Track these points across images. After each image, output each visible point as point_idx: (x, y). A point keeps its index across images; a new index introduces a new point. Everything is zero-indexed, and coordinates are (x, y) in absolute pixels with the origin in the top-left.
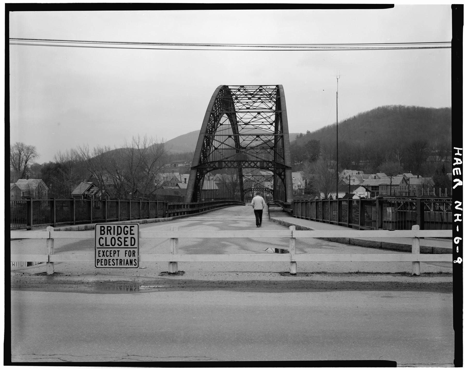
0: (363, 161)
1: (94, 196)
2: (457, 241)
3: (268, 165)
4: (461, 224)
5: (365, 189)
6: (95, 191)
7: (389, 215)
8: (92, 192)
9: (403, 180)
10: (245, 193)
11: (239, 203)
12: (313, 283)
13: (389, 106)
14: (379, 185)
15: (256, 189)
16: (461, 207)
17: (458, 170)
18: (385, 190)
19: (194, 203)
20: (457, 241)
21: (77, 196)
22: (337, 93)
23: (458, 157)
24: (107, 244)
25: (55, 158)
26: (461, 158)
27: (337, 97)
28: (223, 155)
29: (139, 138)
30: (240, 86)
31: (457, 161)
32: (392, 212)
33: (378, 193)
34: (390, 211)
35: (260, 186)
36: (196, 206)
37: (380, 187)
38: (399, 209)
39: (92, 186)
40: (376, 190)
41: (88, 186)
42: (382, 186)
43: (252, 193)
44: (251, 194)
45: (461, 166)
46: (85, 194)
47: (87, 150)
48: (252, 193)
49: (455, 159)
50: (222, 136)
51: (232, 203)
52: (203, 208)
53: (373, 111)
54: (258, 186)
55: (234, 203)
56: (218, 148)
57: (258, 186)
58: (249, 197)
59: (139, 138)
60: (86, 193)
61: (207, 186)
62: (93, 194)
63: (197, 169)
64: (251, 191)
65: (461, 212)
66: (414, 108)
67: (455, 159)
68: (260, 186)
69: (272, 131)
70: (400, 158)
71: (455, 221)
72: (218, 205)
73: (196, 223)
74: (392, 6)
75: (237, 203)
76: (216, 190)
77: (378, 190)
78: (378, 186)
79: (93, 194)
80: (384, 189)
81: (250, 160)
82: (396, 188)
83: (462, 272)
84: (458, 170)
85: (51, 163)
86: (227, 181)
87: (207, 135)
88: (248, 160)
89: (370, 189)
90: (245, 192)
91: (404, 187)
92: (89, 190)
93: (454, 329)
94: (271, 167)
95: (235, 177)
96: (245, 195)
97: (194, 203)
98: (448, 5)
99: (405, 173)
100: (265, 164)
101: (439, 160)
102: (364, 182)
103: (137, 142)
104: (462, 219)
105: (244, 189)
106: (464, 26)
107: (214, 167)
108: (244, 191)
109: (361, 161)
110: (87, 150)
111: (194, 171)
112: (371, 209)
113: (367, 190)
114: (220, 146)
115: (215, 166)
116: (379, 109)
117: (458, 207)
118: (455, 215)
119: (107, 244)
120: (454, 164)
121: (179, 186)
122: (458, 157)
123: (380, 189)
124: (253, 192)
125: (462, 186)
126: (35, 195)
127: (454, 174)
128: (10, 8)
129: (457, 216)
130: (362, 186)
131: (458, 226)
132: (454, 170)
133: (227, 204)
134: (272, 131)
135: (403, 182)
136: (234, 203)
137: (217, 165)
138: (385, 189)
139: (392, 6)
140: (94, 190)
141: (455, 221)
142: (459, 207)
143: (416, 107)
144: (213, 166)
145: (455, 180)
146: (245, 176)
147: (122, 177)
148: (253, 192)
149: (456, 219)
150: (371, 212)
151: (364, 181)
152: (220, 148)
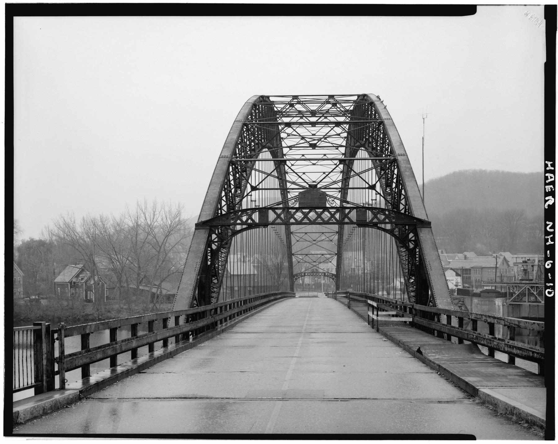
0: (441, 238)
1: (84, 284)
3: (375, 216)
5: (454, 273)
6: (86, 278)
7: (499, 309)
8: (82, 279)
9: (503, 261)
10: (296, 279)
11: (288, 295)
13: (467, 171)
14: (471, 267)
15: (312, 274)
18: (479, 273)
19: (202, 308)
20: (548, 265)
21: (62, 285)
22: (423, 138)
24: (18, 21)
25: (42, 234)
27: (423, 145)
29: (146, 203)
30: (293, 96)
31: (549, 177)
32: (503, 305)
33: (470, 278)
34: (500, 304)
35: (316, 270)
36: (208, 313)
37: (472, 269)
38: (512, 301)
39: (82, 271)
40: (467, 274)
41: (75, 271)
42: (475, 269)
47: (73, 220)
50: (263, 191)
51: (279, 296)
52: (225, 316)
53: (447, 177)
55: (283, 295)
56: (258, 187)
57: (314, 270)
59: (146, 203)
60: (74, 280)
62: (83, 281)
63: (211, 226)
65: (554, 233)
66: (497, 172)
70: (488, 235)
72: (257, 303)
74: (470, 10)
75: (286, 295)
76: (254, 275)
77: (470, 274)
78: (470, 270)
79: (83, 281)
80: (478, 273)
81: (333, 205)
82: (489, 271)
85: (32, 240)
86: (269, 263)
87: (234, 160)
88: (328, 206)
89: (459, 272)
90: (296, 277)
91: (505, 271)
92: (77, 276)
94: (383, 222)
96: (296, 282)
97: (202, 308)
99: (501, 251)
100: (369, 215)
101: (539, 236)
102: (450, 264)
103: (143, 208)
105: (294, 273)
107: (250, 221)
108: (294, 277)
109: (438, 238)
110: (73, 220)
111: (204, 231)
112: (472, 300)
113: (457, 275)
114: (261, 185)
115: (252, 220)
116: (455, 174)
119: (18, 21)
120: (547, 182)
123: (472, 272)
130: (451, 269)
132: (547, 187)
133: (272, 298)
135: (503, 264)
136: (283, 295)
137: (256, 217)
138: (479, 272)
139: (470, 10)
140: (84, 277)
142: (550, 228)
143: (501, 172)
144: (247, 220)
145: (547, 198)
147: (124, 258)
150: (471, 305)
151: (449, 262)
152: (261, 187)
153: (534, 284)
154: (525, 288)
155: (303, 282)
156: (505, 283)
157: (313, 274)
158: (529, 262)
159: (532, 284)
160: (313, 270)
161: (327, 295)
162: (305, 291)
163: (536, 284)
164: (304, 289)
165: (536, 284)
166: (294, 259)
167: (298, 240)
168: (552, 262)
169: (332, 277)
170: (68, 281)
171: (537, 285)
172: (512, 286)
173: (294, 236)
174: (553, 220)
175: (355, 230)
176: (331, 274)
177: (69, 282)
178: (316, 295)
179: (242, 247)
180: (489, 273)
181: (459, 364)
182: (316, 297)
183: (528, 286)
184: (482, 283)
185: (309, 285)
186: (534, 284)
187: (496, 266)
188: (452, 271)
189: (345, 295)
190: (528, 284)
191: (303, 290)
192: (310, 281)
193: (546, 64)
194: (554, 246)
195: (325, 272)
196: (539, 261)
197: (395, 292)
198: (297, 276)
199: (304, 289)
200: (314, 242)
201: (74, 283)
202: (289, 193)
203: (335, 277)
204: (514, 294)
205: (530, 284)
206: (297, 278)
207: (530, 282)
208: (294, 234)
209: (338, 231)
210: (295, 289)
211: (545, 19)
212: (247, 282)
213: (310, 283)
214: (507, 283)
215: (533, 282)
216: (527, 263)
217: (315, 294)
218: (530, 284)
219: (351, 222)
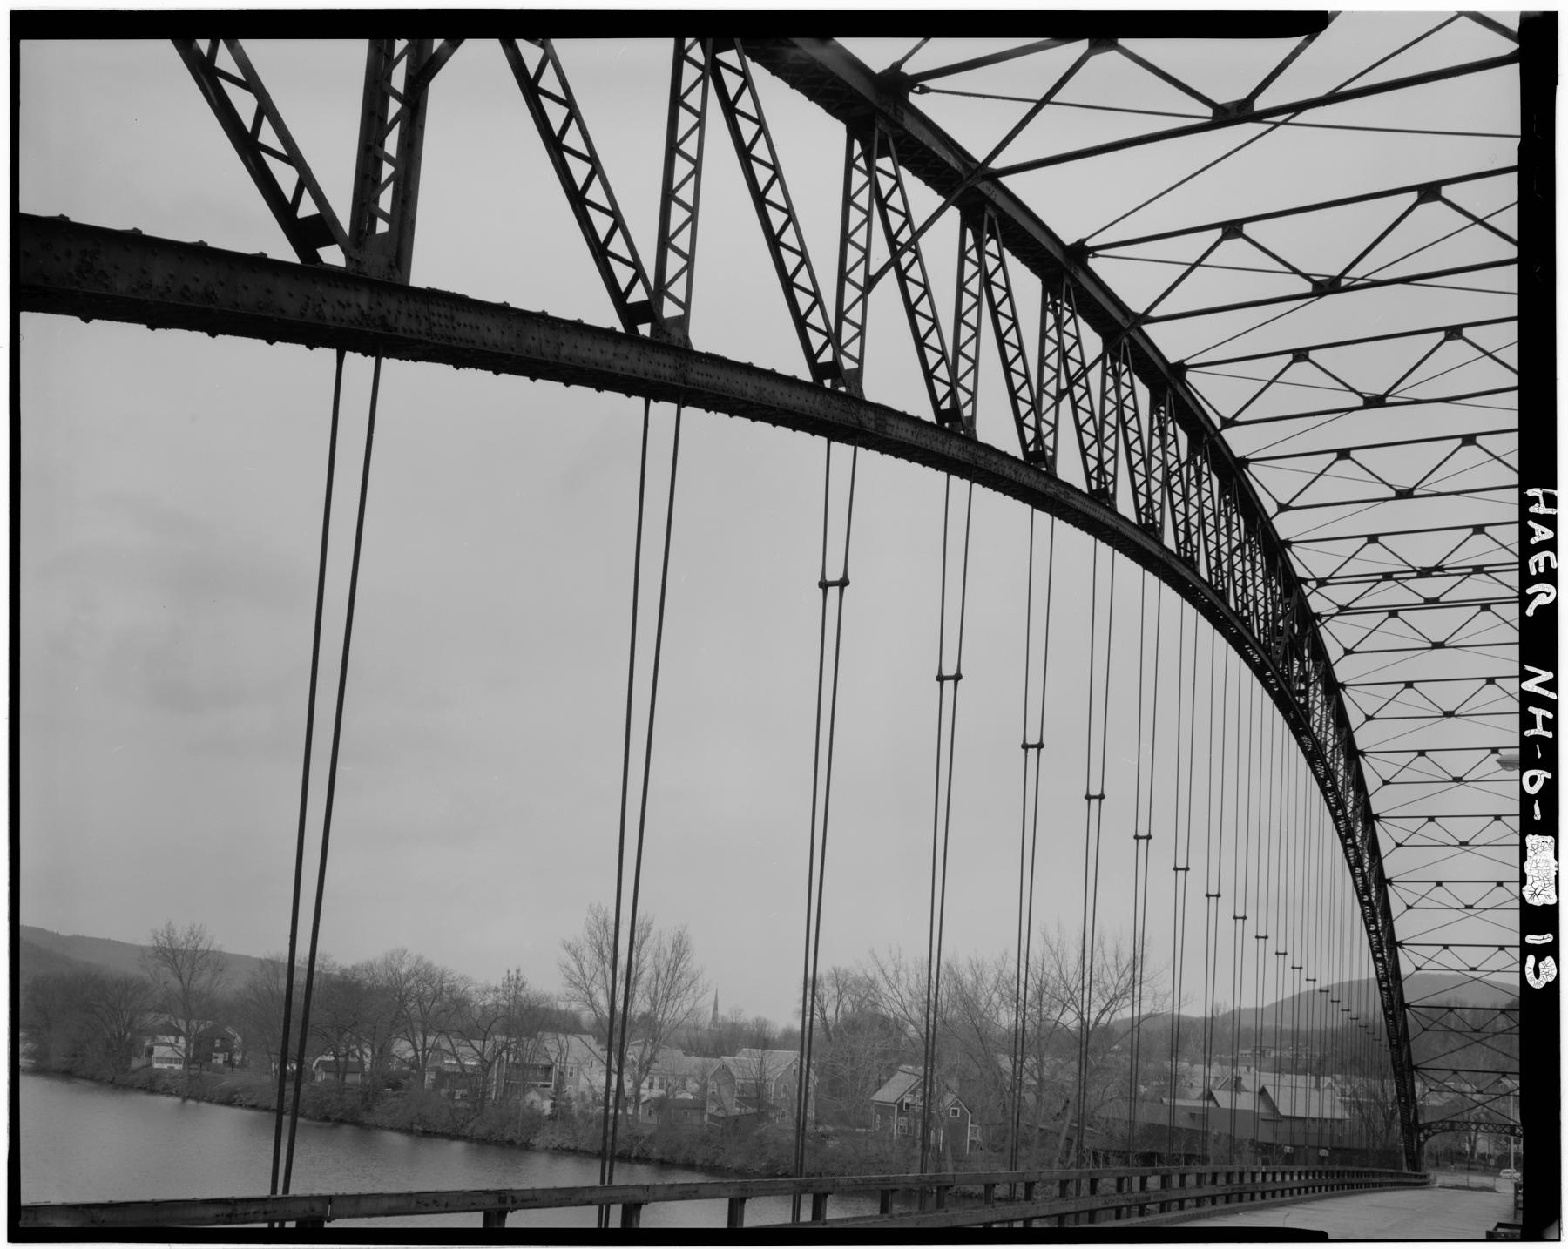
10: (1427, 1137)
12: (470, 345)
16: (1552, 685)
21: (885, 1109)
28: (1377, 1037)
43: (1470, 1139)
44: (1467, 1146)
46: (903, 1101)
48: (1470, 1139)
54: (1482, 1116)
57: (1482, 1116)
58: (1460, 1154)
60: (908, 1100)
64: (1468, 1130)
65: (1553, 706)
68: (1487, 1115)
69: (1452, 970)
73: (1188, 1221)
83: (1555, 82)
90: (1426, 1131)
96: (1426, 1146)
98: (1514, 13)
104: (1557, 693)
106: (1559, 88)
117: (1538, 685)
121: (1214, 1099)
124: (1475, 1138)
125: (1556, 907)
126: (775, 1090)
127: (1533, 572)
134: (1452, 970)
141: (1530, 612)
148: (1475, 1138)
149: (1534, 535)
155: (1473, 1148)
160: (1478, 1115)
162: (1472, 1169)
167: (1426, 1026)
168: (1549, 776)
170: (893, 1101)
177: (895, 1103)
182: (1491, 1190)
187: (484, 1043)
191: (1469, 1169)
192: (1492, 1147)
193: (1557, 84)
194: (1554, 743)
195: (1512, 1123)
198: (1430, 1129)
200: (1477, 1036)
201: (907, 1105)
202: (1391, 884)
217: (1487, 1180)
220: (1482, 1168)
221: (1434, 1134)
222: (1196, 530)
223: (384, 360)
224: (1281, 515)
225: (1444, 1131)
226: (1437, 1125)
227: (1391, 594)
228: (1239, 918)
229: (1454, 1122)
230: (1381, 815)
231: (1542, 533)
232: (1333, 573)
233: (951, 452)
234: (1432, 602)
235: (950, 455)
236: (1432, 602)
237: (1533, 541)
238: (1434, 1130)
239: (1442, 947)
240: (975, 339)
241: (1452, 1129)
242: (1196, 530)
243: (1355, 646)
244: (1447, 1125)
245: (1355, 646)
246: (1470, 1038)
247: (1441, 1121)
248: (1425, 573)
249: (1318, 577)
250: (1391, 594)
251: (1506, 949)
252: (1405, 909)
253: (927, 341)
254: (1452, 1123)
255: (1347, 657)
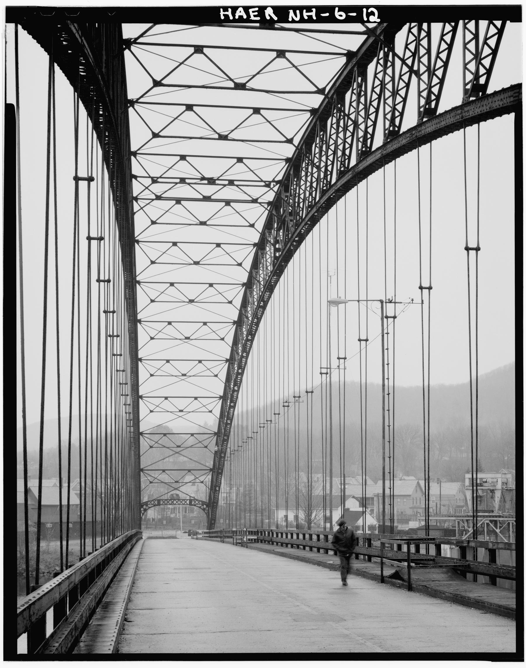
2: (341, 16)
4: (320, 9)
17: (253, 12)
20: (341, 16)
23: (234, 14)
24: (512, 648)
26: (234, 9)
31: (241, 14)
45: (246, 9)
49: (237, 17)
57: (175, 495)
61: (99, 472)
67: (237, 17)
71: (315, 18)
83: (492, 661)
84: (253, 12)
90: (145, 507)
93: (401, 28)
95: (143, 517)
108: (142, 506)
118: (306, 18)
119: (512, 648)
122: (234, 14)
128: (517, 657)
129: (224, 15)
130: (354, 497)
131: (321, 15)
132: (253, 18)
135: (416, 490)
145: (268, 18)
146: (146, 439)
153: (496, 517)
154: (484, 523)
156: (452, 516)
157: (172, 502)
158: (485, 484)
159: (493, 517)
160: (172, 495)
161: (192, 534)
163: (500, 516)
164: (148, 526)
165: (500, 516)
166: (143, 479)
169: (202, 507)
171: (501, 519)
172: (462, 520)
173: (146, 439)
174: (216, 10)
175: (264, 427)
176: (201, 503)
178: (174, 535)
179: (259, 412)
180: (399, 503)
181: (312, 631)
182: (174, 537)
183: (486, 521)
184: (419, 515)
185: (153, 520)
186: (496, 517)
188: (355, 499)
189: (208, 535)
190: (487, 516)
192: (156, 514)
194: (317, 7)
196: (503, 483)
197: (64, 543)
198: (147, 505)
199: (148, 526)
203: (207, 506)
204: (464, 533)
205: (490, 516)
206: (147, 508)
207: (491, 514)
208: (145, 435)
209: (216, 431)
210: (143, 527)
211: (25, 30)
212: (97, 508)
213: (156, 517)
214: (455, 516)
215: (494, 514)
216: (482, 486)
218: (490, 516)
219: (187, 504)
220: (154, 526)
221: (149, 508)
222: (316, 155)
223: (508, 22)
224: (154, 139)
225: (154, 506)
226: (151, 503)
227: (182, 191)
228: (309, 392)
229: (160, 500)
230: (142, 320)
231: (240, 13)
232: (162, 175)
233: (476, 112)
234: (207, 199)
235: (476, 114)
236: (207, 199)
237: (245, 17)
238: (149, 506)
239: (164, 399)
240: (488, 37)
241: (159, 504)
242: (316, 155)
243: (157, 220)
244: (156, 502)
245: (157, 220)
246: (173, 451)
247: (153, 500)
248: (211, 181)
249: (152, 176)
250: (182, 191)
251: (169, 399)
252: (150, 376)
253: (473, 36)
254: (159, 501)
255: (153, 226)
